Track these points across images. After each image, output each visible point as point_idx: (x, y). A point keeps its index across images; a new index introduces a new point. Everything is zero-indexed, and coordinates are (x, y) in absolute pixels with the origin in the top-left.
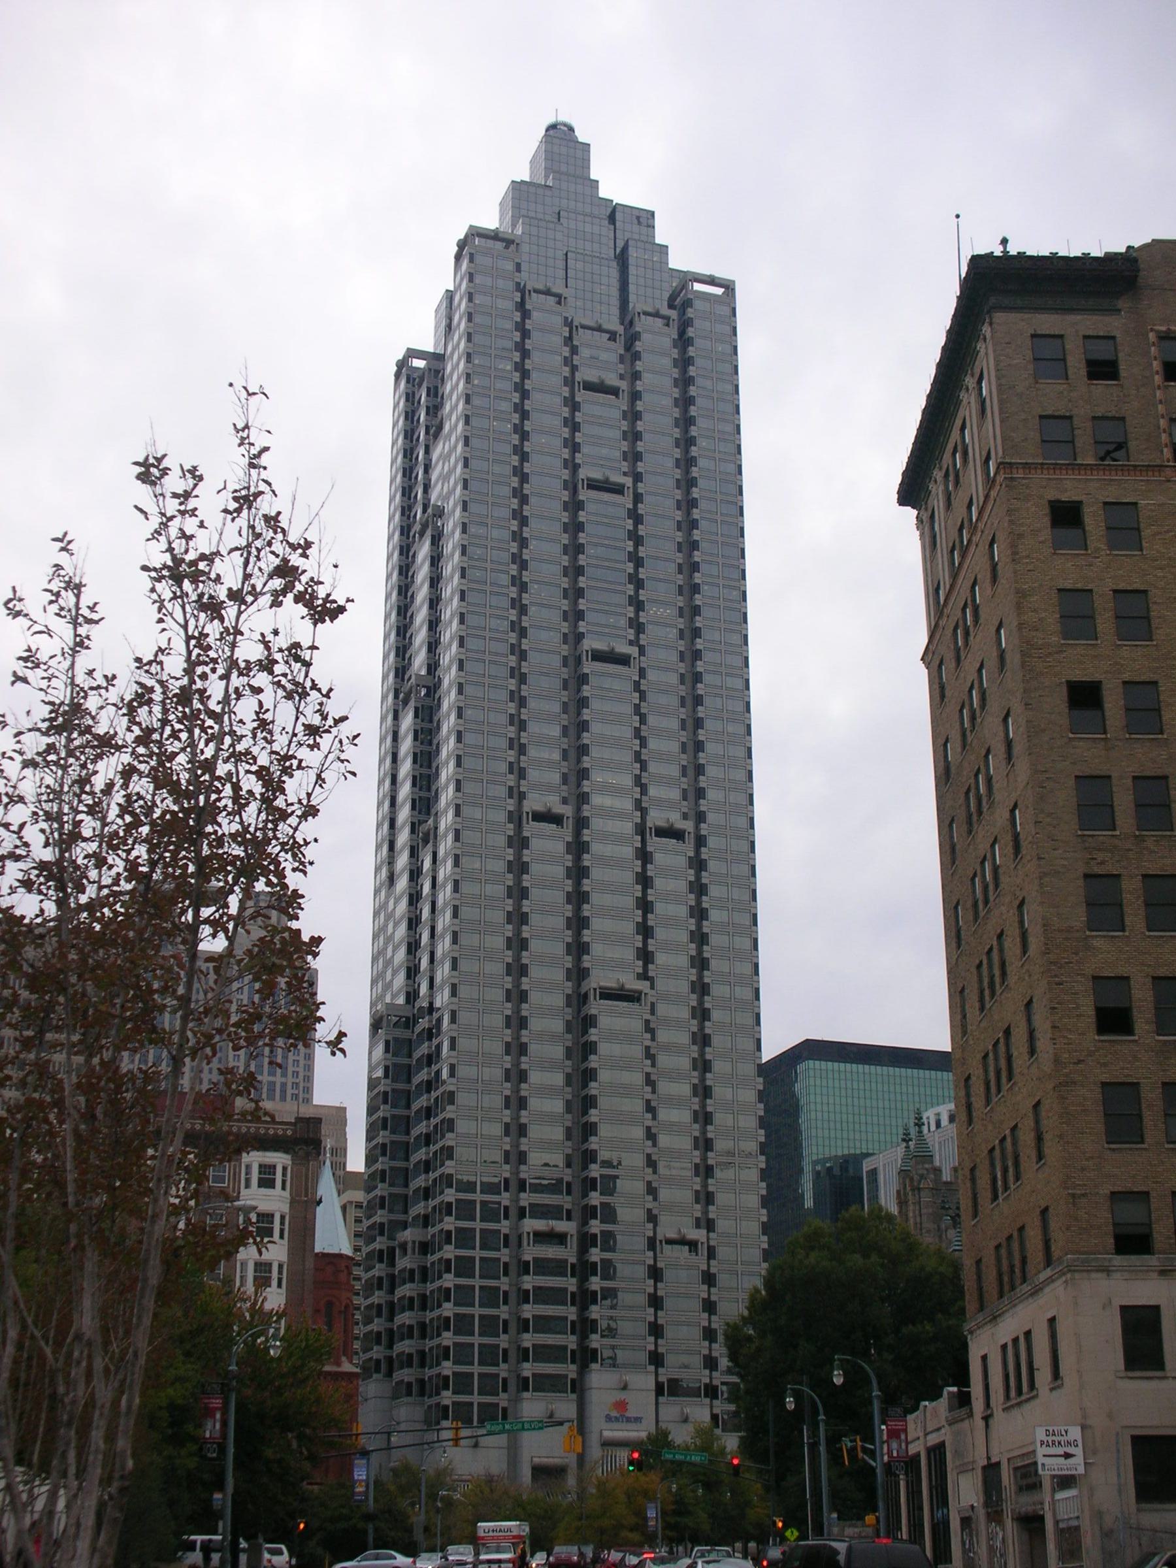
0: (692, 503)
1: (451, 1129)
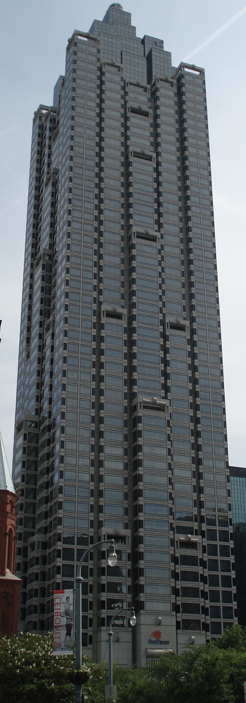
0: (190, 251)
1: (60, 524)
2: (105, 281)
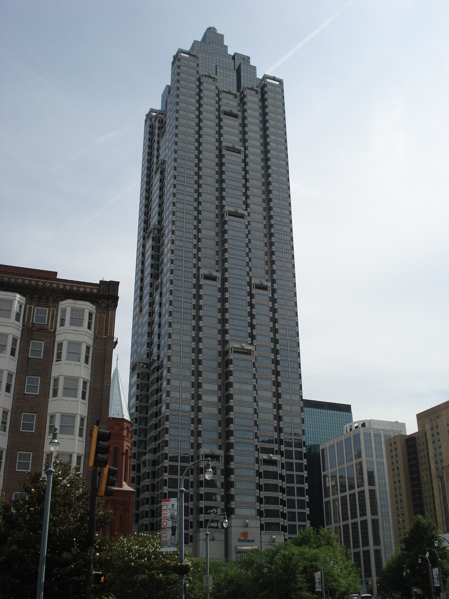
2: (203, 250)
